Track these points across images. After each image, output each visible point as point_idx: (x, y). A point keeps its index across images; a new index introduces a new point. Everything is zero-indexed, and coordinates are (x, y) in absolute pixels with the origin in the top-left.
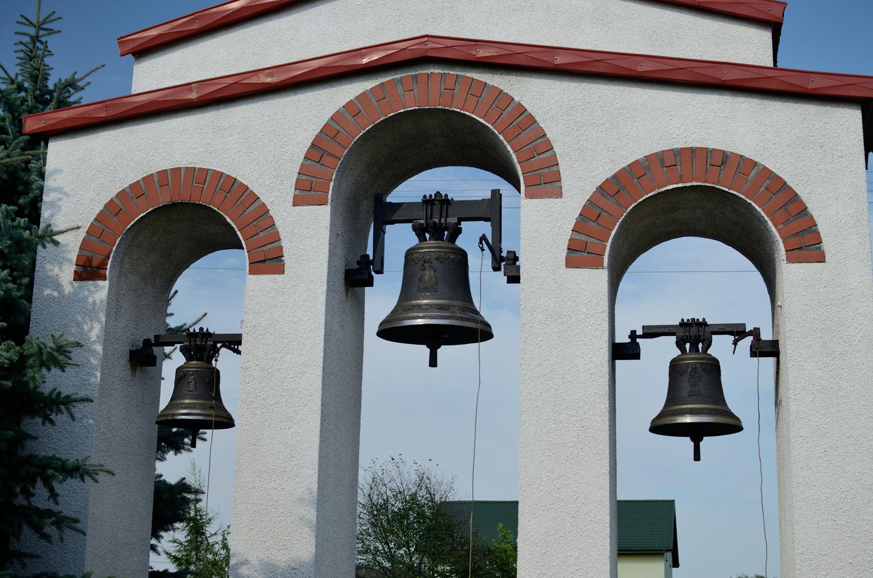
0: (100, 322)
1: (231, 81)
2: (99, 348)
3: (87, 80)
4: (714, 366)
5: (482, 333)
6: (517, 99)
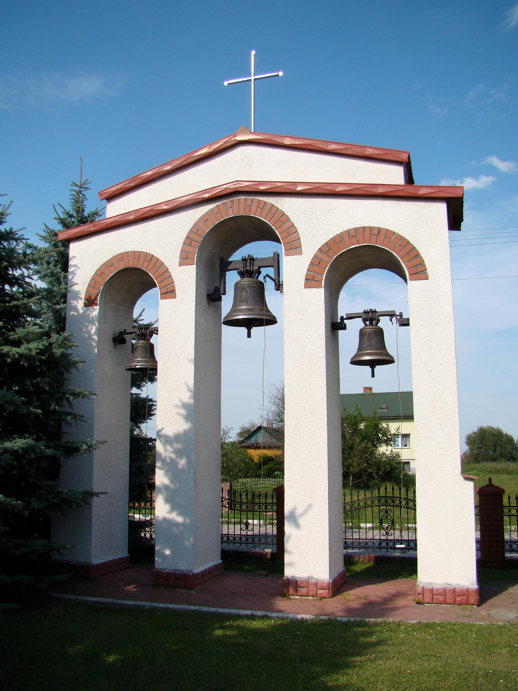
0: (96, 325)
1: (148, 209)
2: (95, 337)
3: (103, 211)
4: (380, 333)
5: (271, 321)
6: (280, 209)
